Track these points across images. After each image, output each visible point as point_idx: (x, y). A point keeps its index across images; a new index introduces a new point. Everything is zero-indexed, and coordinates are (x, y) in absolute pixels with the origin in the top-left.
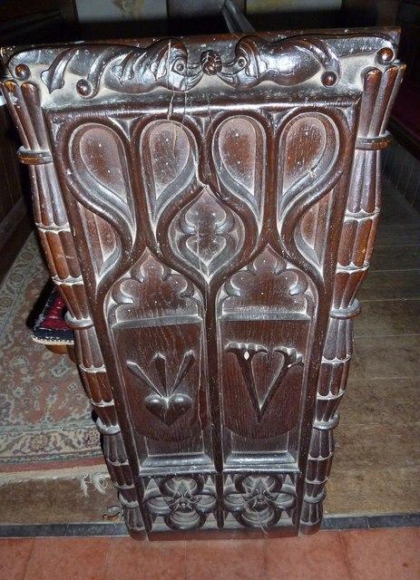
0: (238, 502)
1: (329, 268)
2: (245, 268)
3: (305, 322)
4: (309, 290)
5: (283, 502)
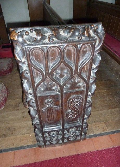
2: (43, 83)
4: (58, 88)
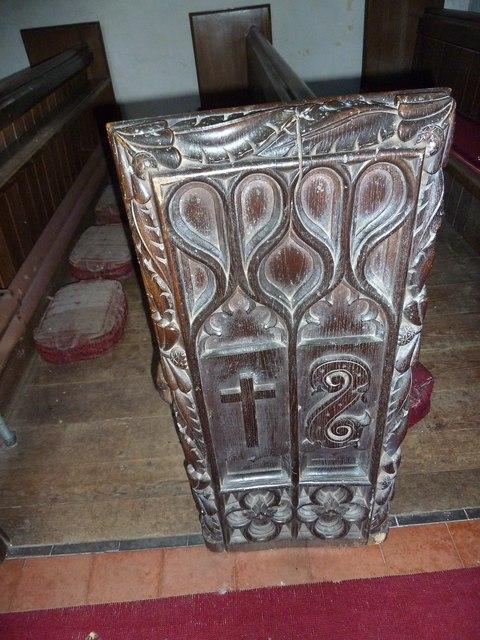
0: (307, 513)
1: (399, 296)
2: (324, 299)
3: (376, 344)
5: (353, 514)
